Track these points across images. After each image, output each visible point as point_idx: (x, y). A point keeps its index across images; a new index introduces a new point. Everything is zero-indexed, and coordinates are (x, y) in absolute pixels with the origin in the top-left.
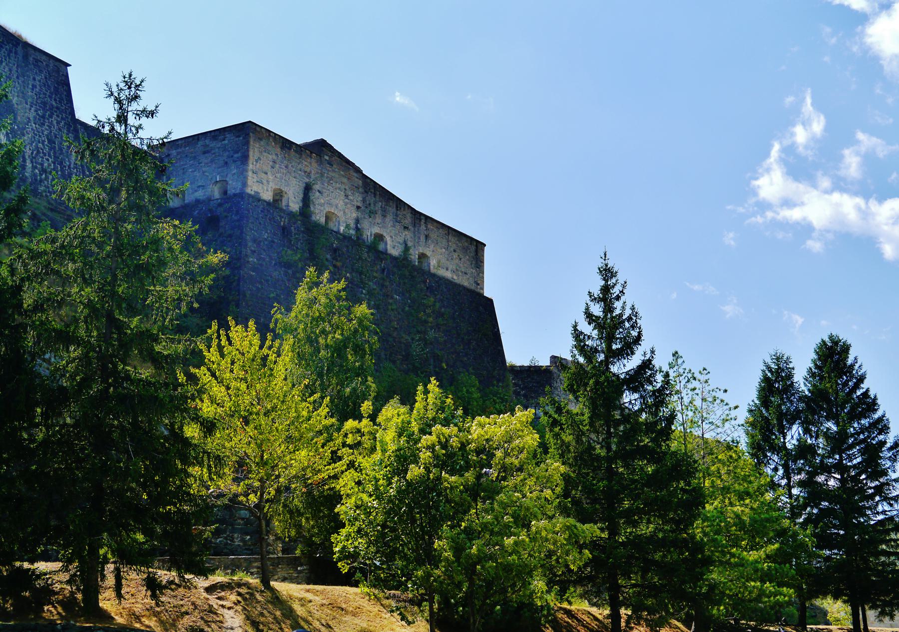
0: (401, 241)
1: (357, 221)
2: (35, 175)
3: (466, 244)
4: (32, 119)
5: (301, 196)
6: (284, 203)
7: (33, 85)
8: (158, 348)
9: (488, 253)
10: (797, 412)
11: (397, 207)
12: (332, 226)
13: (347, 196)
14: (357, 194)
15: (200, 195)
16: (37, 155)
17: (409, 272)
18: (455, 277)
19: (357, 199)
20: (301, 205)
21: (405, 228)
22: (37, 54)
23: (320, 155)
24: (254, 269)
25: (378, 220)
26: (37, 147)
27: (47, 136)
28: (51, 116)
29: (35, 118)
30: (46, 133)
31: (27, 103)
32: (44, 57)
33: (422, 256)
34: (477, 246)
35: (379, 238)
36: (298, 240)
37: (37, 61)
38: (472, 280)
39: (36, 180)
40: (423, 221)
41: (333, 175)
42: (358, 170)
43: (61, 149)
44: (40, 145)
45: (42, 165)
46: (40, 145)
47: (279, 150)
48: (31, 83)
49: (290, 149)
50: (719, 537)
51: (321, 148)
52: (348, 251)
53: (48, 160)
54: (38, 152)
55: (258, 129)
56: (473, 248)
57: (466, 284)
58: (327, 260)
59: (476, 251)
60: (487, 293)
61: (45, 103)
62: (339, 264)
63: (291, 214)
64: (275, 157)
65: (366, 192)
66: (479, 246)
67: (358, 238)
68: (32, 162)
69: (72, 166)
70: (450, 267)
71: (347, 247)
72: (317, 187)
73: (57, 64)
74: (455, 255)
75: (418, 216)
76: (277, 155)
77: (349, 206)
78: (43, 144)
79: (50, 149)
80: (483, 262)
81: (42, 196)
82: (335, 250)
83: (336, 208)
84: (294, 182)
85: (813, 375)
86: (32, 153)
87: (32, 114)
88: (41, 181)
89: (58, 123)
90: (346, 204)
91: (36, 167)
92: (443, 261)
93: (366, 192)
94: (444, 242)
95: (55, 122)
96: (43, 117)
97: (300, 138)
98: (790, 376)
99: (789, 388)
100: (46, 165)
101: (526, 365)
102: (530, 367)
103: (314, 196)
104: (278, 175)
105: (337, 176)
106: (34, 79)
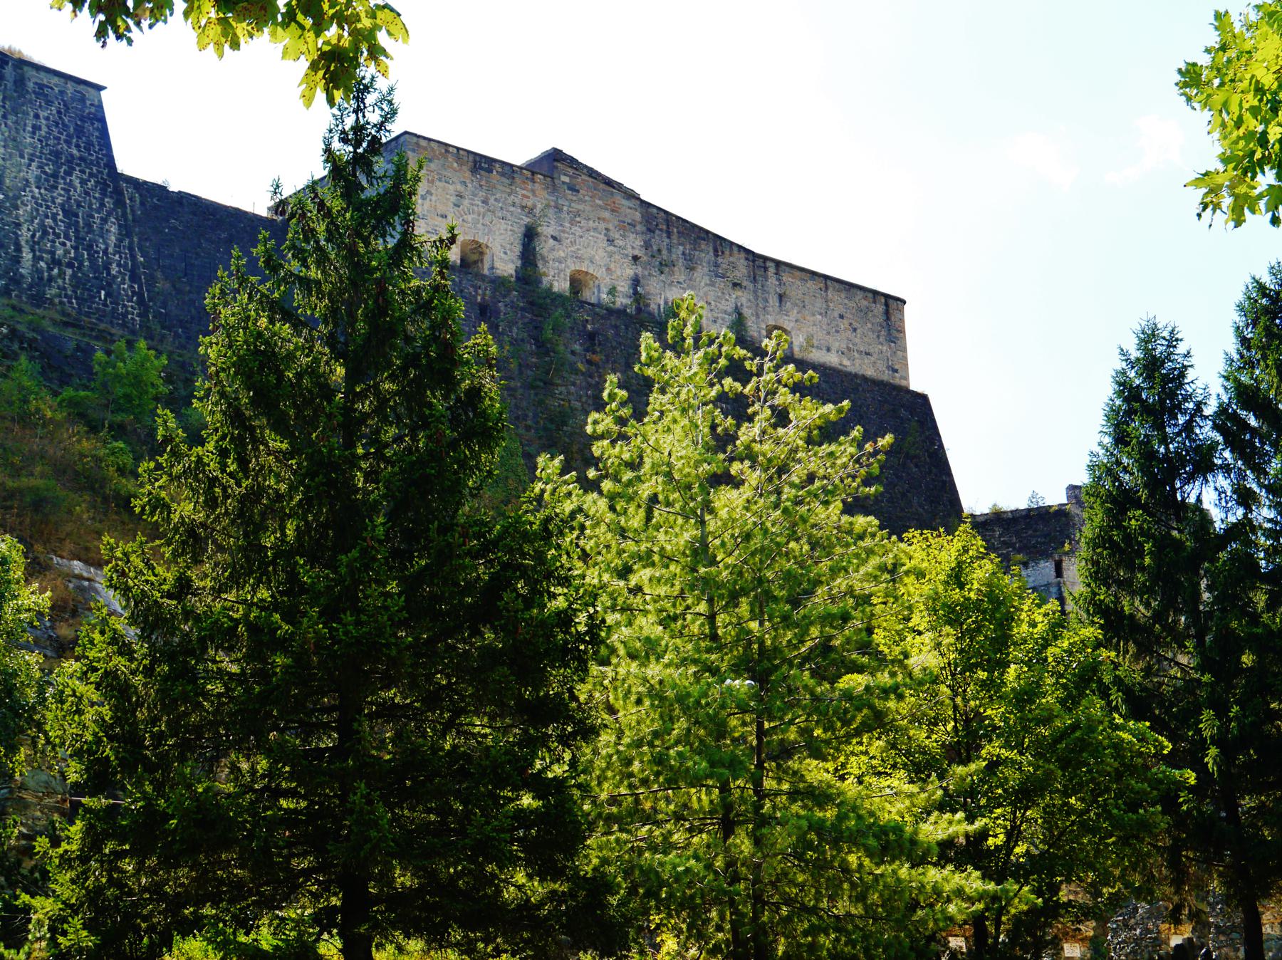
0: (729, 309)
1: (636, 282)
2: (40, 271)
3: (865, 303)
4: (32, 180)
5: (518, 249)
6: (487, 265)
7: (34, 127)
8: (1148, 724)
9: (912, 318)
11: (716, 251)
12: (589, 295)
13: (611, 241)
14: (632, 236)
16: (42, 238)
18: (846, 362)
19: (634, 244)
20: (519, 263)
21: (735, 285)
22: (42, 75)
23: (550, 176)
25: (680, 274)
26: (42, 225)
27: (62, 206)
28: (69, 173)
29: (38, 178)
30: (59, 200)
31: (22, 156)
32: (56, 80)
34: (887, 305)
36: (512, 323)
37: (41, 86)
38: (881, 365)
39: (41, 279)
40: (772, 270)
41: (581, 207)
42: (631, 195)
43: (89, 225)
44: (49, 222)
45: (52, 253)
46: (49, 222)
47: (468, 174)
48: (30, 123)
49: (490, 171)
50: (355, 553)
52: (617, 334)
53: (64, 244)
54: (45, 233)
55: (423, 143)
56: (880, 308)
57: (870, 372)
58: (573, 353)
59: (887, 313)
60: (915, 386)
61: (57, 154)
62: (596, 358)
63: (498, 283)
64: (460, 187)
65: (649, 230)
66: (891, 306)
67: (639, 310)
68: (33, 250)
69: (111, 250)
70: (835, 346)
71: (616, 327)
72: (547, 230)
73: (81, 88)
74: (843, 324)
75: (760, 262)
76: (464, 183)
77: (617, 257)
78: (55, 219)
79: (68, 227)
80: (902, 331)
81: (52, 303)
82: (592, 336)
86: (33, 236)
87: (33, 173)
88: (51, 279)
89: (83, 182)
90: (611, 255)
91: (41, 258)
92: (819, 336)
93: (649, 230)
94: (819, 304)
95: (77, 183)
96: (55, 175)
97: (519, 153)
100: (60, 252)
101: (1022, 507)
102: (1029, 510)
103: (545, 247)
104: (469, 218)
105: (588, 208)
106: (37, 116)
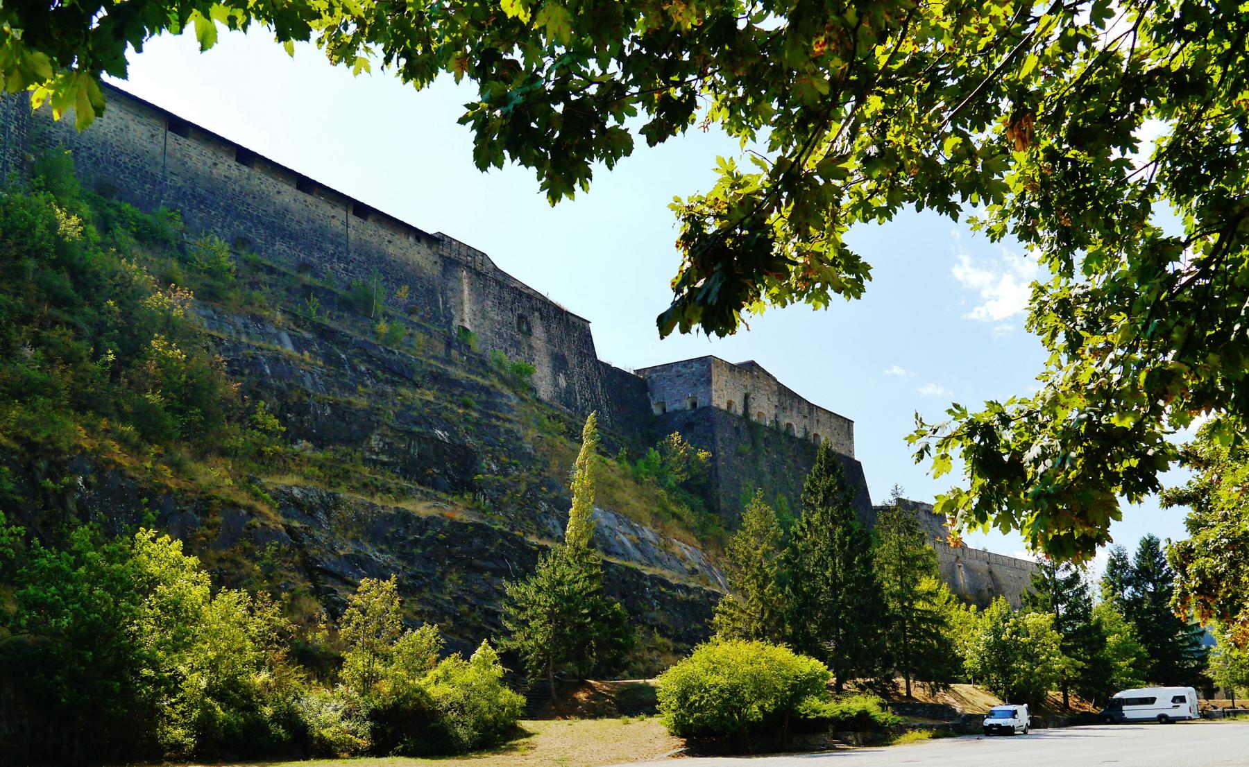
1: (776, 416)
10: (1131, 579)
15: (677, 406)
17: (807, 447)
19: (775, 400)
24: (724, 460)
33: (816, 435)
35: (789, 425)
42: (775, 380)
51: (751, 367)
60: (857, 458)
83: (764, 409)
84: (738, 394)
85: (1139, 557)
98: (1125, 558)
99: (1125, 566)
